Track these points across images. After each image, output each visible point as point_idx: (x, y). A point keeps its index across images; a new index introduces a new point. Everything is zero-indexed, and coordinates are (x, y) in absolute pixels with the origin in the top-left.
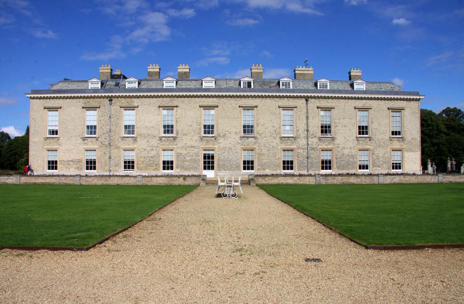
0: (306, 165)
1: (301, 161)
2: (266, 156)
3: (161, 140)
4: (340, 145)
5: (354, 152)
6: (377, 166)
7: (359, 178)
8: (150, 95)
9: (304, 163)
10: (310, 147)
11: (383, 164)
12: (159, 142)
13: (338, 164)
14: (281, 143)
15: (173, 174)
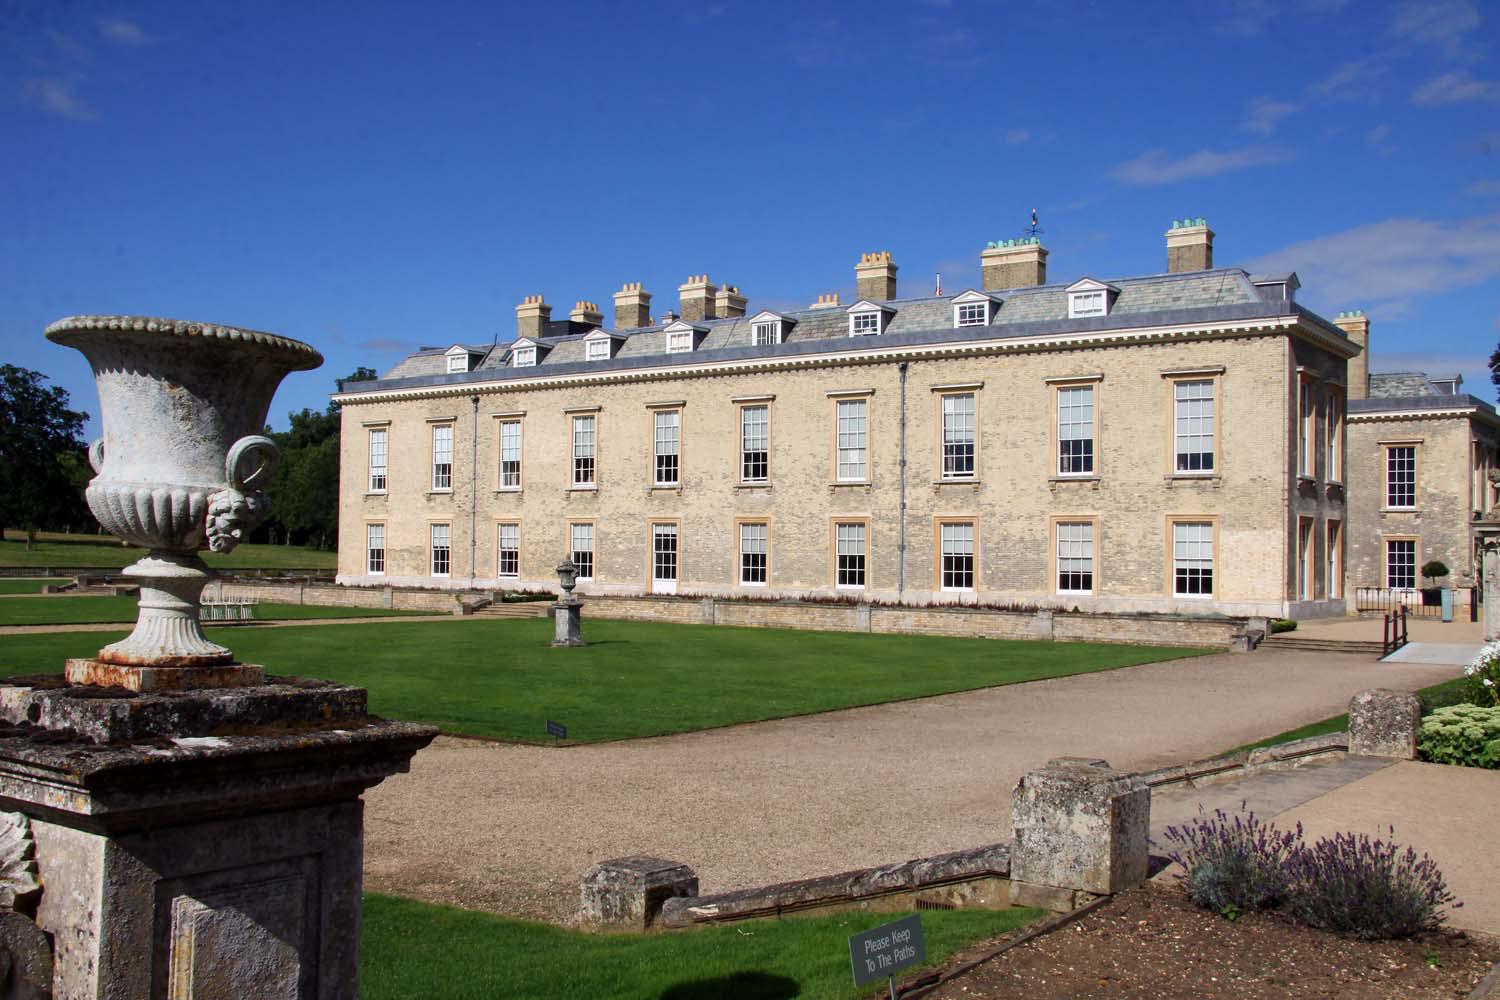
0: (895, 569)
1: (884, 557)
3: (568, 497)
4: (997, 507)
5: (1040, 529)
6: (1117, 580)
7: (807, 612)
8: (1165, 335)
9: (891, 564)
10: (910, 516)
13: (990, 569)
14: (832, 504)
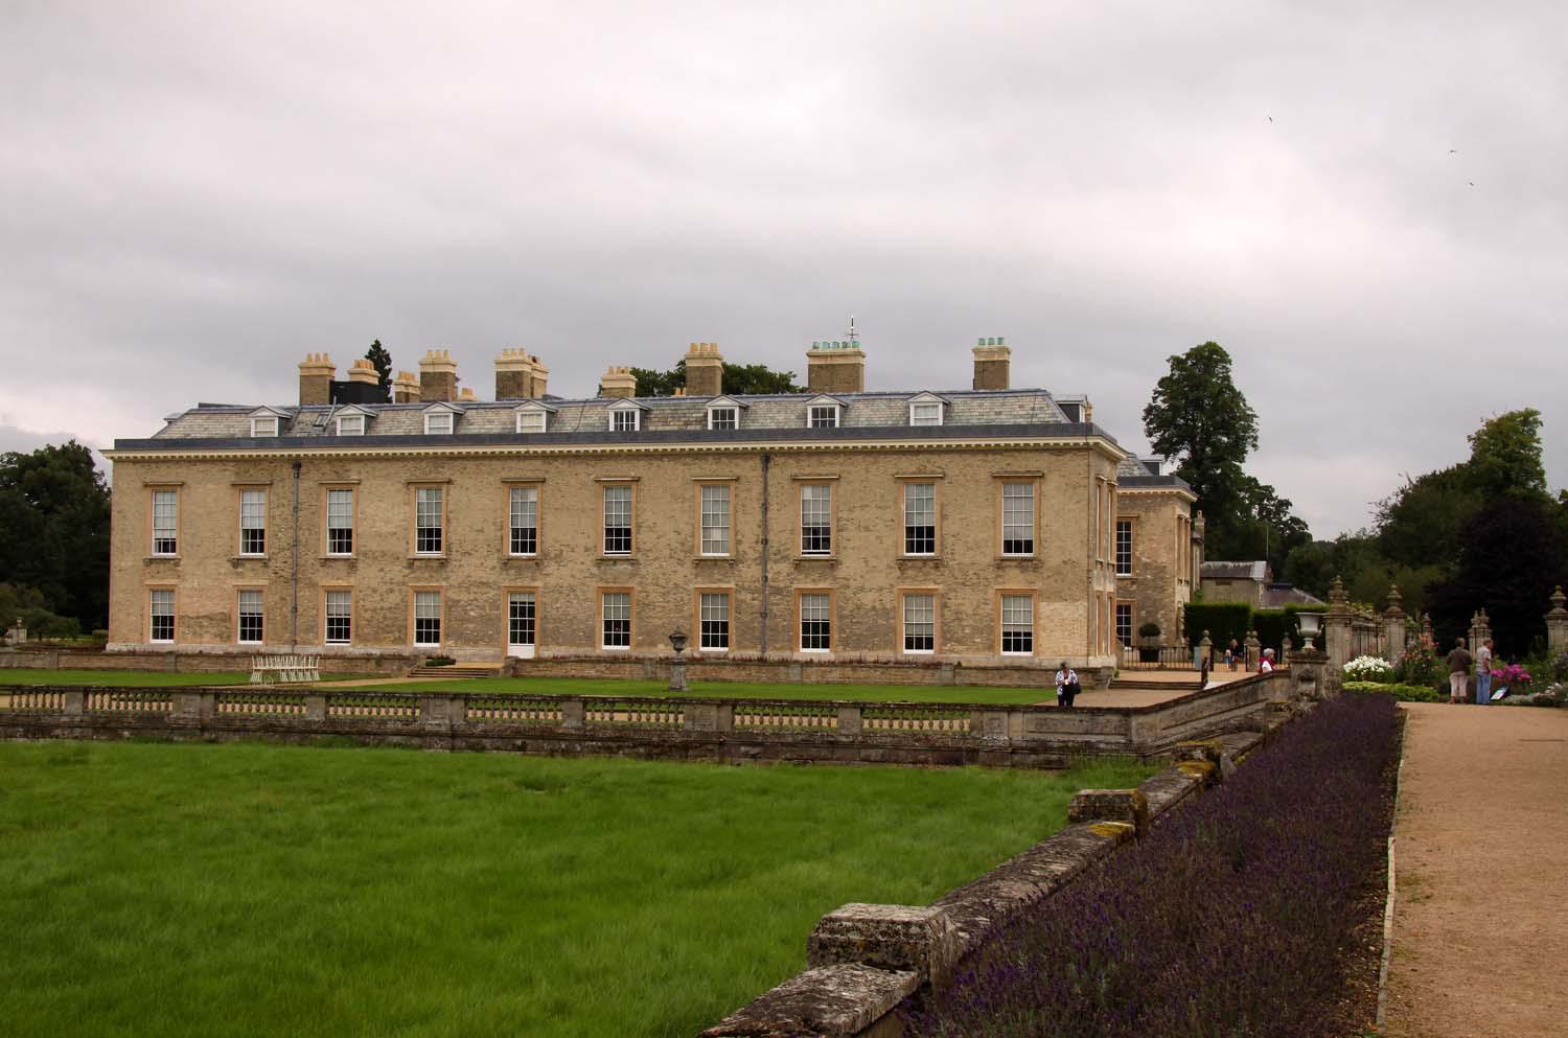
2: (658, 609)
5: (888, 599)
9: (754, 629)
11: (972, 636)
12: (407, 571)
14: (696, 576)
15: (263, 650)
